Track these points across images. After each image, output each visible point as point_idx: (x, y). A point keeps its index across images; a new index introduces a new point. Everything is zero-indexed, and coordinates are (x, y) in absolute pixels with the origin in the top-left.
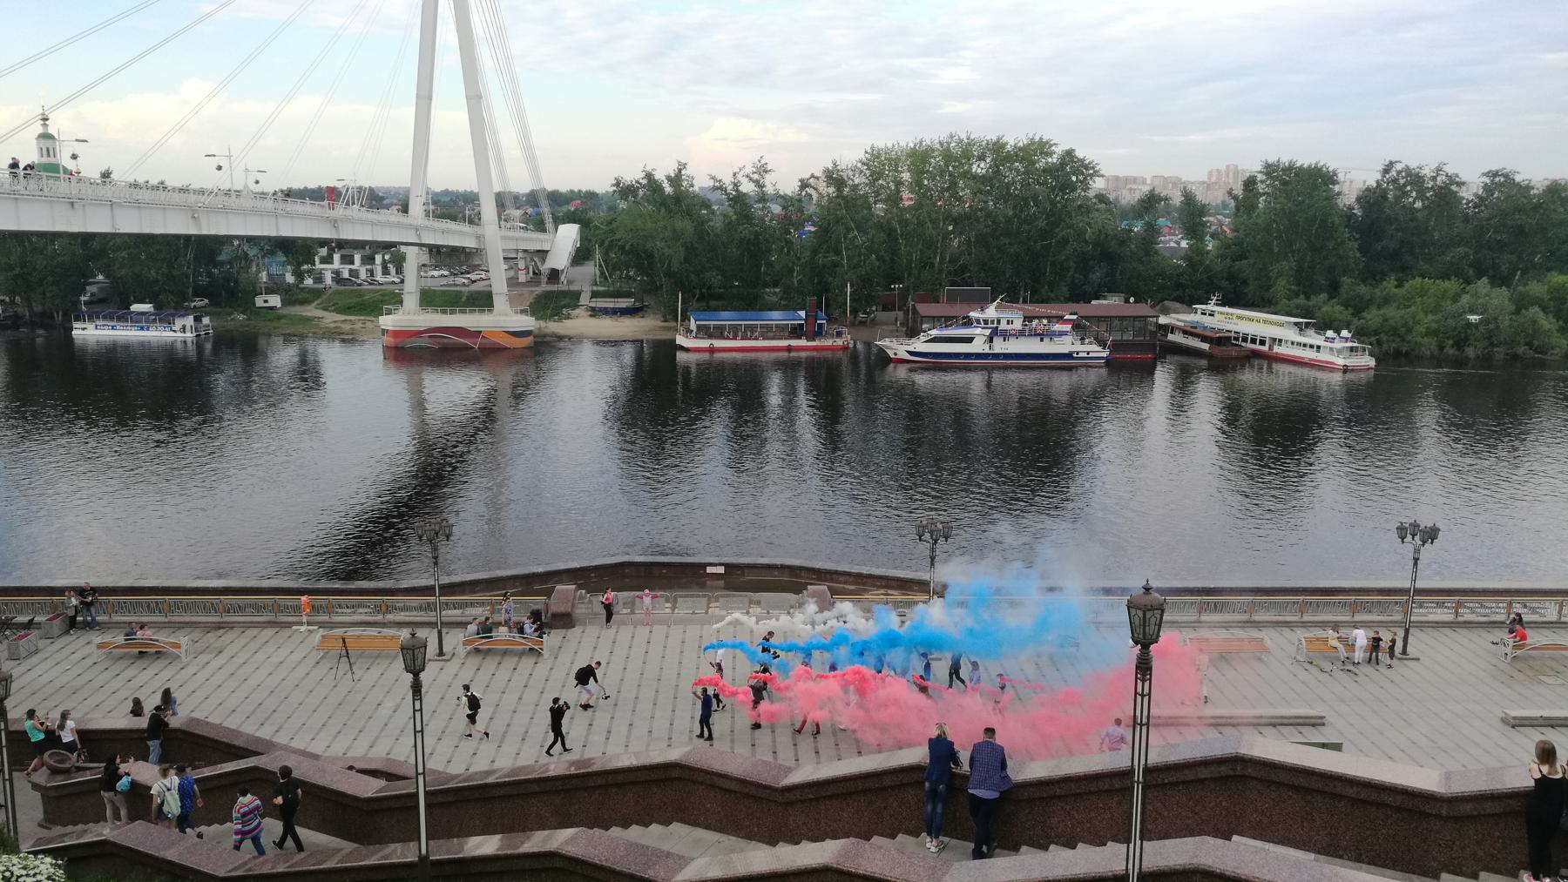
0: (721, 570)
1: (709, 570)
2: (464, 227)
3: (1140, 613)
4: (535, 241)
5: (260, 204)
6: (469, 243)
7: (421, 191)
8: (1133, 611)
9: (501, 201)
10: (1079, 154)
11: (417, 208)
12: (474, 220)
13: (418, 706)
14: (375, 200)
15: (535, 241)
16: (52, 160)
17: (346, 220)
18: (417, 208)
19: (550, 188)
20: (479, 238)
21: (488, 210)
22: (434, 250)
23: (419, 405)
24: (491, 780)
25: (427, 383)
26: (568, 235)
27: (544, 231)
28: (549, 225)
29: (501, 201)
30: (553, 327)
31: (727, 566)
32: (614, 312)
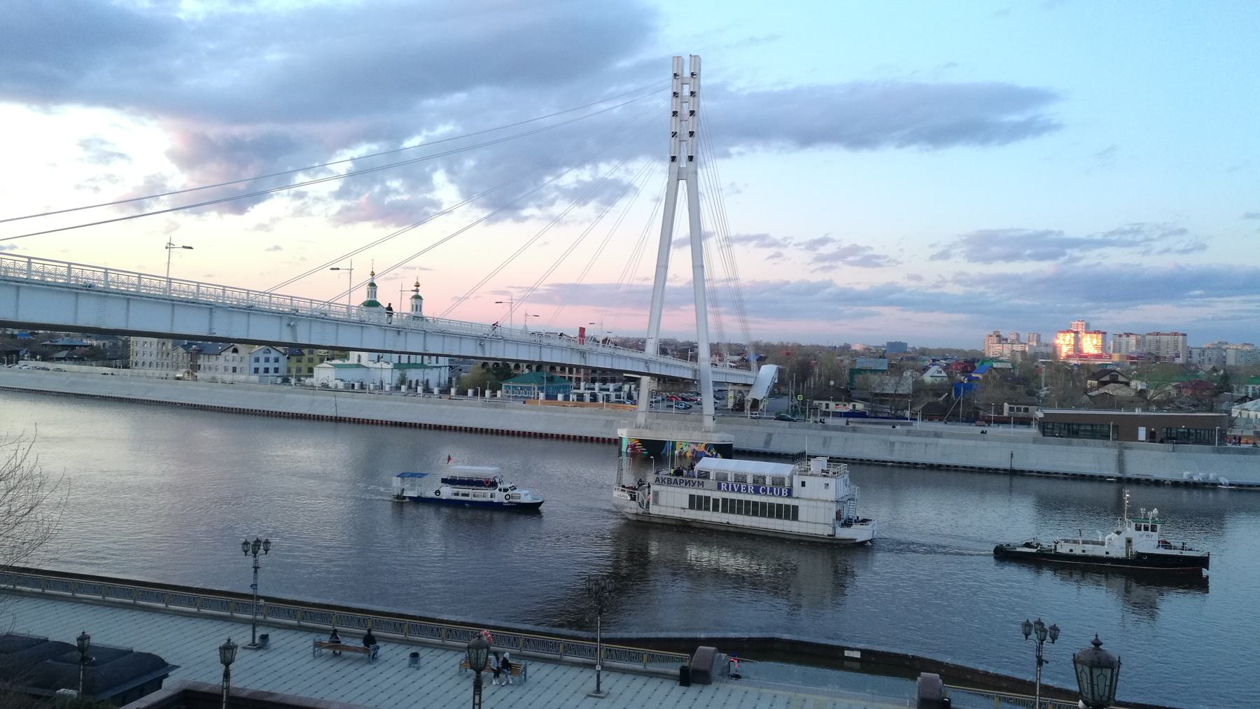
0: (857, 655)
1: (847, 653)
3: (1087, 669)
4: (740, 376)
5: (532, 338)
8: (1080, 667)
9: (715, 350)
12: (695, 358)
13: (477, 701)
14: (625, 344)
15: (740, 376)
16: (418, 314)
17: (591, 352)
18: (651, 349)
21: (704, 352)
22: (660, 378)
24: (269, 699)
26: (768, 372)
28: (754, 364)
29: (715, 350)
31: (863, 651)
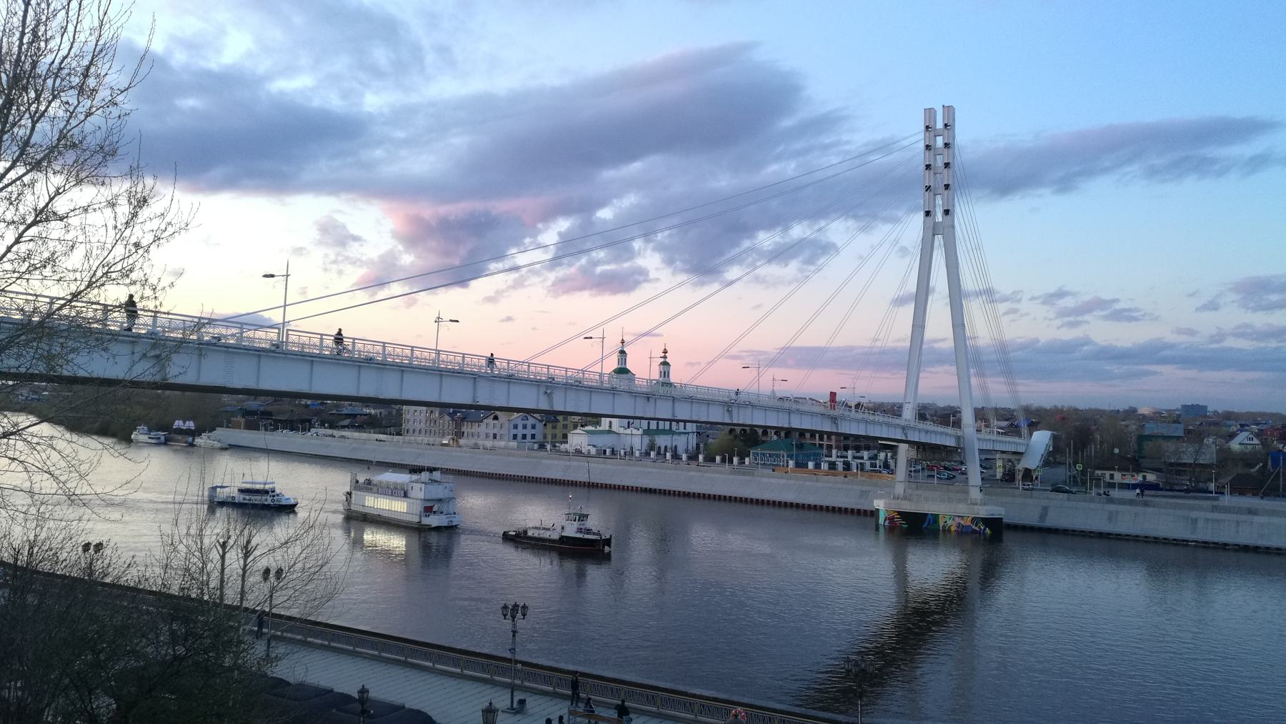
2: (950, 430)
4: (1011, 443)
6: (950, 442)
7: (910, 398)
9: (980, 414)
10: (374, 694)
11: (908, 414)
12: (957, 424)
14: (879, 408)
15: (1011, 443)
17: (843, 418)
18: (908, 414)
19: (1024, 403)
20: (958, 438)
21: (968, 418)
22: (919, 446)
23: (901, 575)
25: (910, 557)
26: (1041, 439)
27: (1020, 435)
28: (1025, 431)
29: (980, 414)
30: (476, 206)
32: (686, 694)
